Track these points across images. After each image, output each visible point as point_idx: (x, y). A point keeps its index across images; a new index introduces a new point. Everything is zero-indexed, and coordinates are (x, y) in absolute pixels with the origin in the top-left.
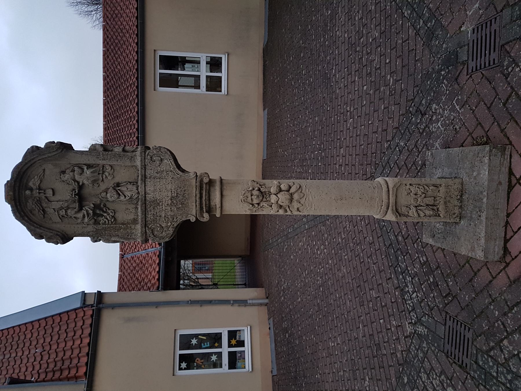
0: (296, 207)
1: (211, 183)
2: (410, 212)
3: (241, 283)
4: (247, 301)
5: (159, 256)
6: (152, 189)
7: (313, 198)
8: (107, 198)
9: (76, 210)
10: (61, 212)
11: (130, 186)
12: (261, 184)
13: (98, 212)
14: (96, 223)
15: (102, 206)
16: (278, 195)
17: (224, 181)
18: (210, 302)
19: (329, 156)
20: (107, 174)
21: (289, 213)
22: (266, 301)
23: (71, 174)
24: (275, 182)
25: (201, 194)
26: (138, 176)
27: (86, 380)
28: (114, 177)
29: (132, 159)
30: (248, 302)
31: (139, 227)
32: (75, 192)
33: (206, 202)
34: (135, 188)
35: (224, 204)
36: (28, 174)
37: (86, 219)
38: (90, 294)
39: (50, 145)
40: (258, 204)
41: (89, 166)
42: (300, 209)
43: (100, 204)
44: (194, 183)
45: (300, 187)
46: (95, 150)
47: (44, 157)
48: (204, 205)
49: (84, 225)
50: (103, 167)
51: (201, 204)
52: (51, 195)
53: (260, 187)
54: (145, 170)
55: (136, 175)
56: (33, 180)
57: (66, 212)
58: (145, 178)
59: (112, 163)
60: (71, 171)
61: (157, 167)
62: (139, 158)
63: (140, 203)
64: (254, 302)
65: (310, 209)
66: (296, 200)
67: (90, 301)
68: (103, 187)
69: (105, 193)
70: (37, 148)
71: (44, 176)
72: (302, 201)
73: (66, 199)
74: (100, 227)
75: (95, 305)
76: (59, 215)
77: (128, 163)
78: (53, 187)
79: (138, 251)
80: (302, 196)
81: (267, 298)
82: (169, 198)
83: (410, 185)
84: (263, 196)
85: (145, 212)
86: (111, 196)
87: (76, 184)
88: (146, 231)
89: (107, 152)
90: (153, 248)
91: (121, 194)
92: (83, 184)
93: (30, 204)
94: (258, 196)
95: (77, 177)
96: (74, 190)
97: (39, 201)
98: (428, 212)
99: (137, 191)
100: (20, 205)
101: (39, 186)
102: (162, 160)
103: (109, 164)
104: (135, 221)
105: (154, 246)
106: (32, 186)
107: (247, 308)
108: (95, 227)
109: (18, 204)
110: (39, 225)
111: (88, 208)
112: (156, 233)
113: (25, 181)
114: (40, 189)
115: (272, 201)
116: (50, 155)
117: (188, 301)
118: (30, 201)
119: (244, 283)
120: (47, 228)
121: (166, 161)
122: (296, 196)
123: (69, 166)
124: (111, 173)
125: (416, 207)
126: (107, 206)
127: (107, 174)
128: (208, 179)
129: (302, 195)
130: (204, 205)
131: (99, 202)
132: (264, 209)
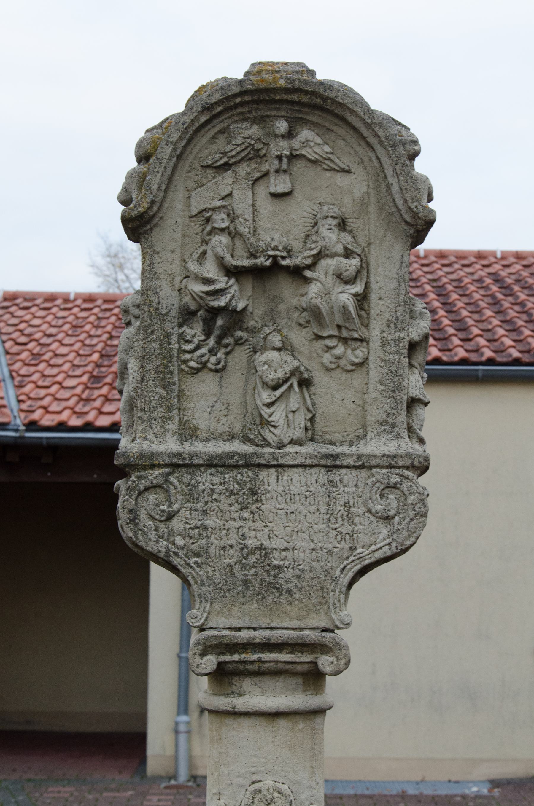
1: (314, 678)
6: (295, 489)
8: (264, 349)
9: (228, 258)
10: (224, 216)
11: (301, 419)
13: (220, 322)
14: (187, 315)
15: (239, 333)
17: (318, 719)
20: (340, 350)
23: (339, 249)
26: (332, 443)
28: (328, 370)
29: (388, 426)
31: (171, 445)
32: (283, 258)
33: (252, 662)
34: (298, 433)
35: (246, 722)
36: (335, 128)
37: (199, 288)
39: (425, 190)
41: (362, 299)
43: (246, 330)
44: (314, 623)
46: (412, 317)
47: (389, 173)
49: (178, 279)
50: (361, 340)
52: (273, 190)
54: (355, 467)
55: (337, 437)
56: (318, 140)
57: (222, 230)
58: (329, 468)
59: (372, 366)
60: (346, 249)
61: (365, 503)
62: (391, 448)
63: (248, 449)
69: (279, 345)
70: (413, 156)
71: (332, 169)
73: (260, 231)
74: (172, 327)
76: (214, 209)
77: (375, 414)
78: (295, 194)
79: (7, 353)
82: (266, 543)
85: (215, 463)
86: (274, 364)
87: (309, 261)
88: (159, 466)
89: (405, 352)
90: (19, 401)
91: (278, 393)
92: (307, 281)
95: (328, 264)
96: (289, 251)
97: (255, 155)
99: (286, 441)
100: (243, 104)
102: (387, 519)
103: (372, 358)
104: (187, 432)
105: (24, 406)
108: (173, 313)
109: (247, 98)
110: (182, 153)
111: (237, 296)
112: (152, 497)
114: (293, 157)
116: (395, 188)
118: (255, 131)
120: (173, 174)
121: (385, 532)
123: (361, 239)
124: (343, 362)
126: (238, 349)
128: (328, 669)
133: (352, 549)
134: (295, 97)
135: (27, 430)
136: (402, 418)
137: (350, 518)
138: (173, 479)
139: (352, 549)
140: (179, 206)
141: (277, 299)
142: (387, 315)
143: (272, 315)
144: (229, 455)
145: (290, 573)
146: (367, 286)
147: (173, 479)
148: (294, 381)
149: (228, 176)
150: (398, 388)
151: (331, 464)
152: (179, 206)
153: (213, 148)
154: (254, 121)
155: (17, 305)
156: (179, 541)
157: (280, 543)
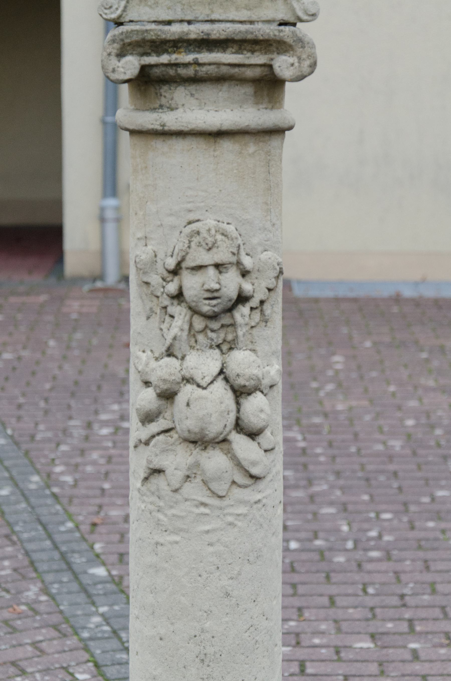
0: (166, 462)
1: (269, 85)
12: (267, 308)
17: (275, 142)
19: (333, 590)
21: (137, 431)
24: (274, 370)
25: (222, 44)
33: (186, 65)
35: (179, 144)
40: (179, 296)
42: (158, 482)
45: (255, 478)
48: (174, 58)
51: (178, 44)
53: (255, 302)
65: (158, 523)
66: (197, 465)
72: (194, 490)
80: (214, 486)
84: (213, 317)
94: (213, 295)
122: (215, 461)
129: (221, 487)
130: (174, 58)
132: (155, 319)
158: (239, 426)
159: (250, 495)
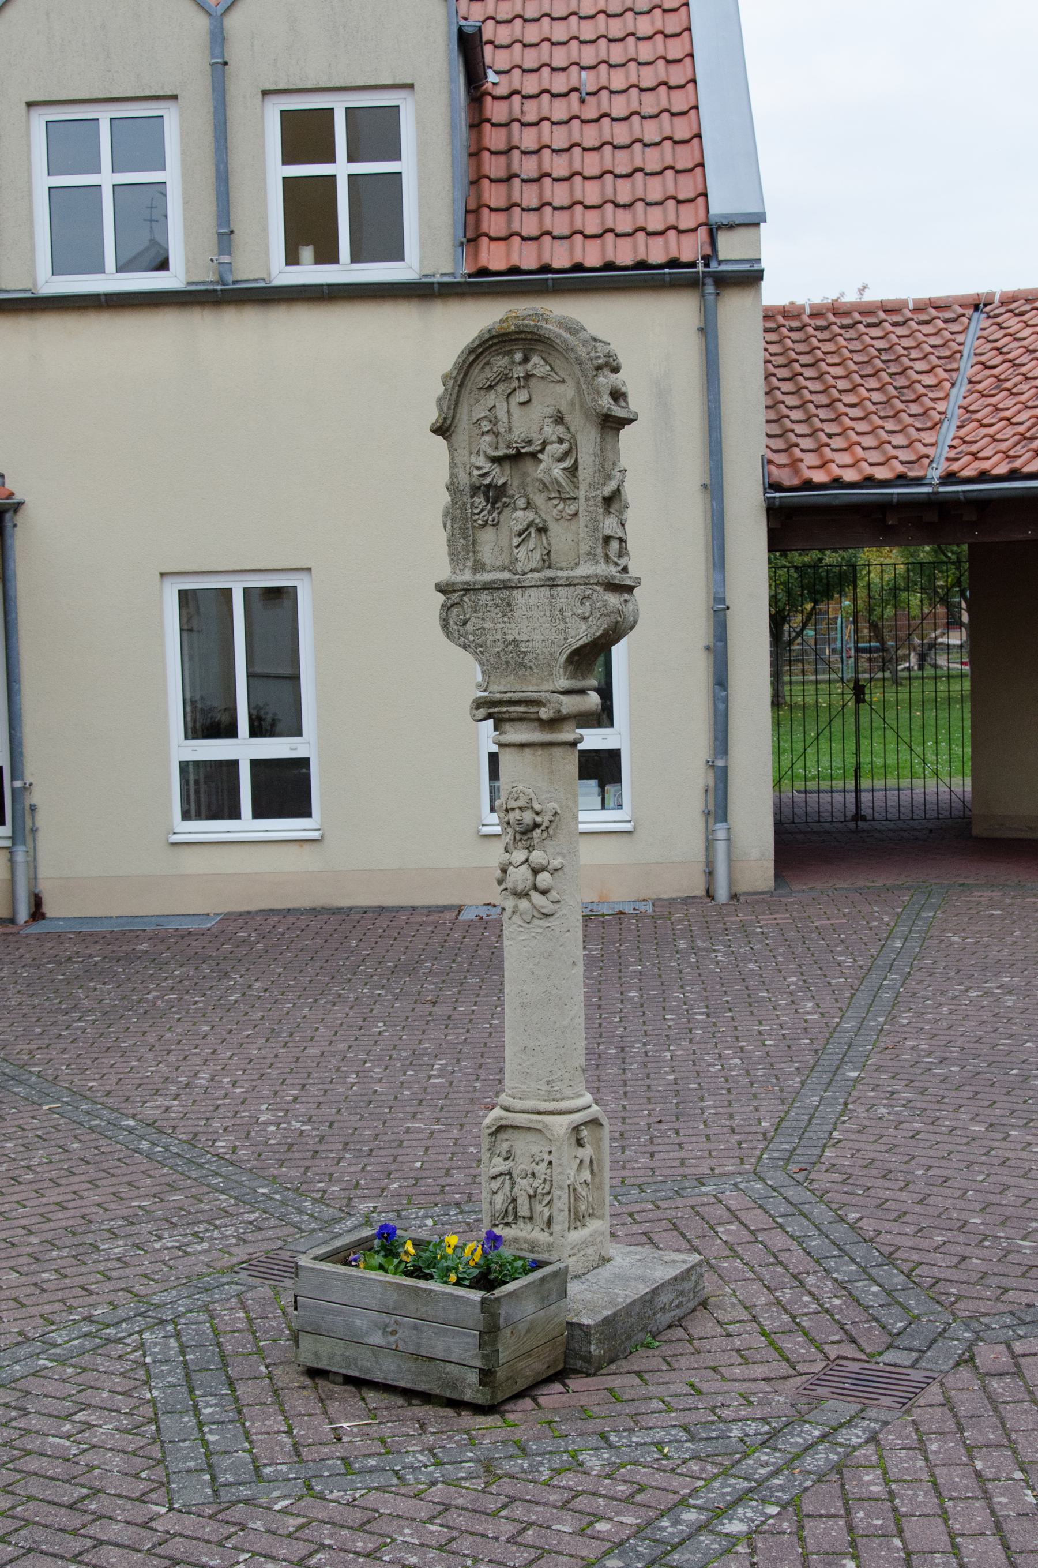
2: (500, 1159)
3: (865, 797)
4: (726, 821)
5: (901, 479)
6: (532, 601)
7: (525, 943)
11: (537, 555)
14: (475, 490)
16: (525, 866)
18: (721, 681)
22: (722, 894)
23: (554, 438)
27: (463, 275)
29: (591, 554)
30: (720, 825)
34: (534, 565)
37: (476, 473)
38: (757, 244)
45: (546, 915)
55: (564, 565)
64: (721, 847)
67: (731, 248)
68: (539, 499)
74: (466, 499)
75: (714, 266)
77: (584, 548)
81: (734, 897)
83: (550, 1163)
85: (489, 587)
86: (521, 518)
92: (541, 461)
93: (500, 362)
94: (520, 822)
97: (506, 378)
98: (499, 1199)
100: (495, 344)
101: (533, 375)
104: (478, 567)
106: (532, 362)
107: (699, 821)
113: (539, 348)
115: (515, 853)
117: (723, 600)
119: (866, 810)
120: (458, 396)
122: (524, 904)
125: (510, 1173)
127: (561, 507)
131: (511, 492)
133: (566, 639)
134: (523, 336)
135: (942, 484)
136: (599, 550)
137: (564, 619)
138: (465, 599)
139: (566, 639)
140: (465, 417)
141: (525, 475)
142: (588, 480)
143: (523, 485)
144: (494, 582)
145: (530, 656)
146: (576, 460)
147: (465, 599)
148: (533, 530)
149: (492, 394)
150: (596, 530)
151: (552, 584)
152: (465, 417)
153: (483, 376)
154: (505, 354)
155: (1011, 311)
156: (471, 638)
157: (525, 638)
158: (535, 888)
159: (544, 923)
